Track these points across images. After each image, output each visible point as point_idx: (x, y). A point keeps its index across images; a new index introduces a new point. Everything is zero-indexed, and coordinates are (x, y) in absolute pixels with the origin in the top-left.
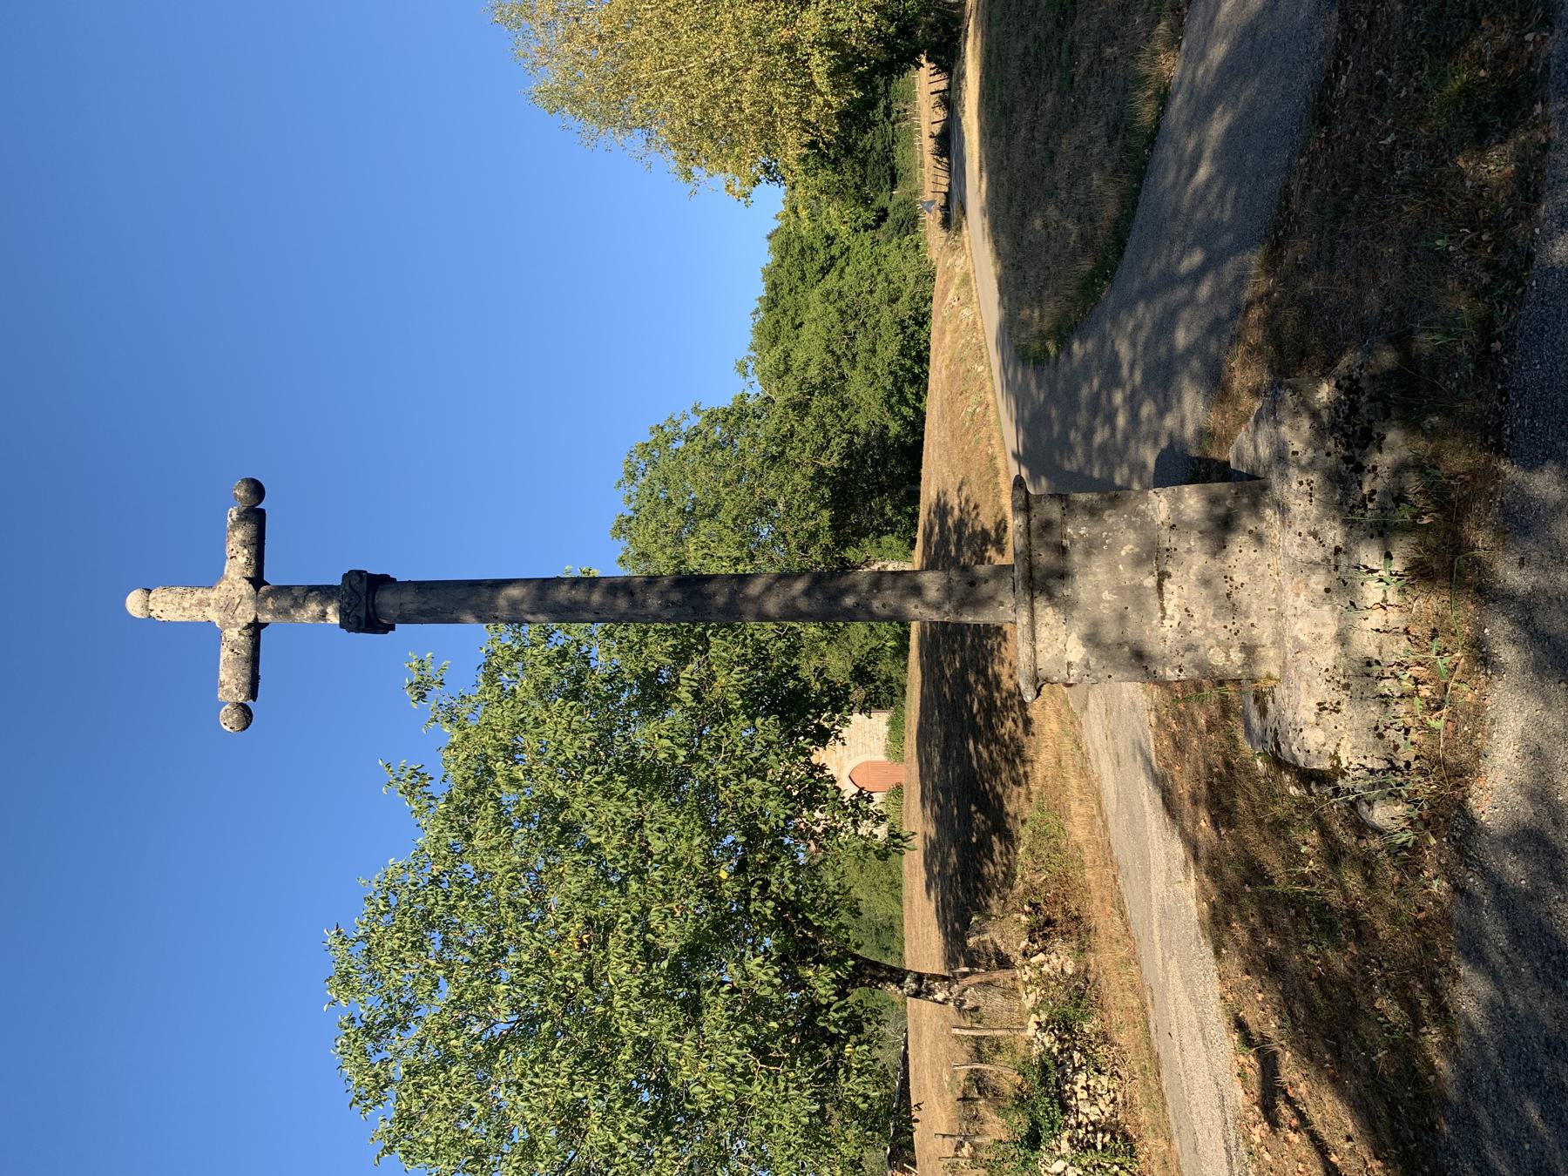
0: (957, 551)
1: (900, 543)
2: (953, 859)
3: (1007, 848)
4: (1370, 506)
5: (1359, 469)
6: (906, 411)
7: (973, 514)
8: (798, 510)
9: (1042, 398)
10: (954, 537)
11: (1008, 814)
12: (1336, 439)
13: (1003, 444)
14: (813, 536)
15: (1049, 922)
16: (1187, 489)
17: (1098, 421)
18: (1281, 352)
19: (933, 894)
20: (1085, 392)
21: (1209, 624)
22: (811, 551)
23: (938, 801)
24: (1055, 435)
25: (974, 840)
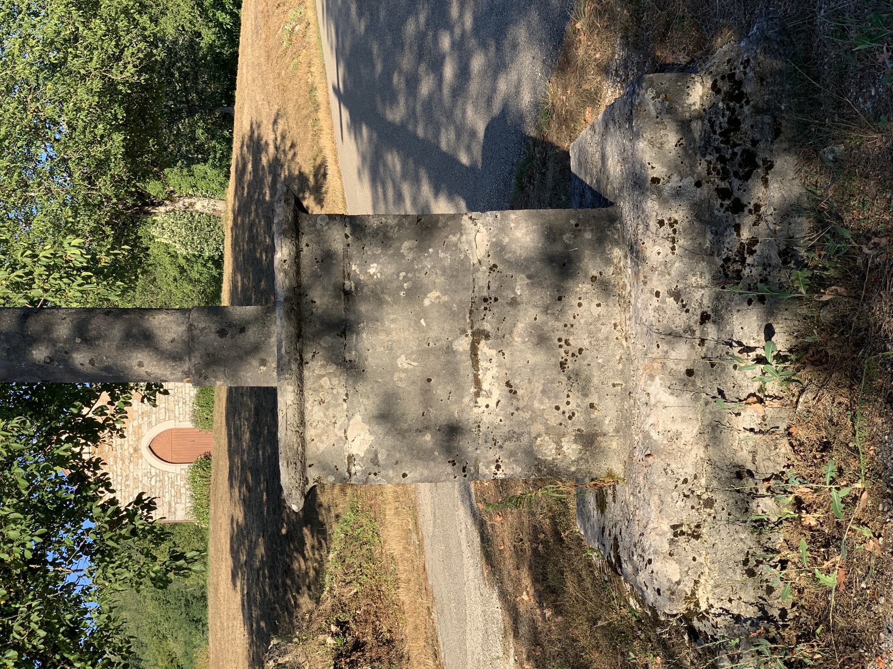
0: (272, 196)
1: (215, 172)
2: (261, 550)
3: (320, 543)
4: (749, 260)
5: (738, 207)
6: (222, 17)
7: (289, 156)
8: (84, 132)
9: (363, 28)
10: (269, 179)
11: (321, 505)
12: (709, 163)
13: (324, 73)
14: (102, 165)
15: (358, 646)
16: (515, 216)
17: (422, 68)
18: (639, 20)
19: (238, 584)
20: (410, 28)
21: (536, 405)
22: (100, 183)
23: (246, 481)
24: (377, 76)
25: (284, 531)
